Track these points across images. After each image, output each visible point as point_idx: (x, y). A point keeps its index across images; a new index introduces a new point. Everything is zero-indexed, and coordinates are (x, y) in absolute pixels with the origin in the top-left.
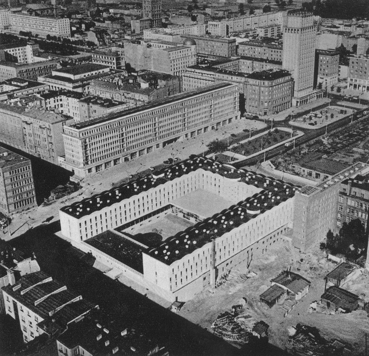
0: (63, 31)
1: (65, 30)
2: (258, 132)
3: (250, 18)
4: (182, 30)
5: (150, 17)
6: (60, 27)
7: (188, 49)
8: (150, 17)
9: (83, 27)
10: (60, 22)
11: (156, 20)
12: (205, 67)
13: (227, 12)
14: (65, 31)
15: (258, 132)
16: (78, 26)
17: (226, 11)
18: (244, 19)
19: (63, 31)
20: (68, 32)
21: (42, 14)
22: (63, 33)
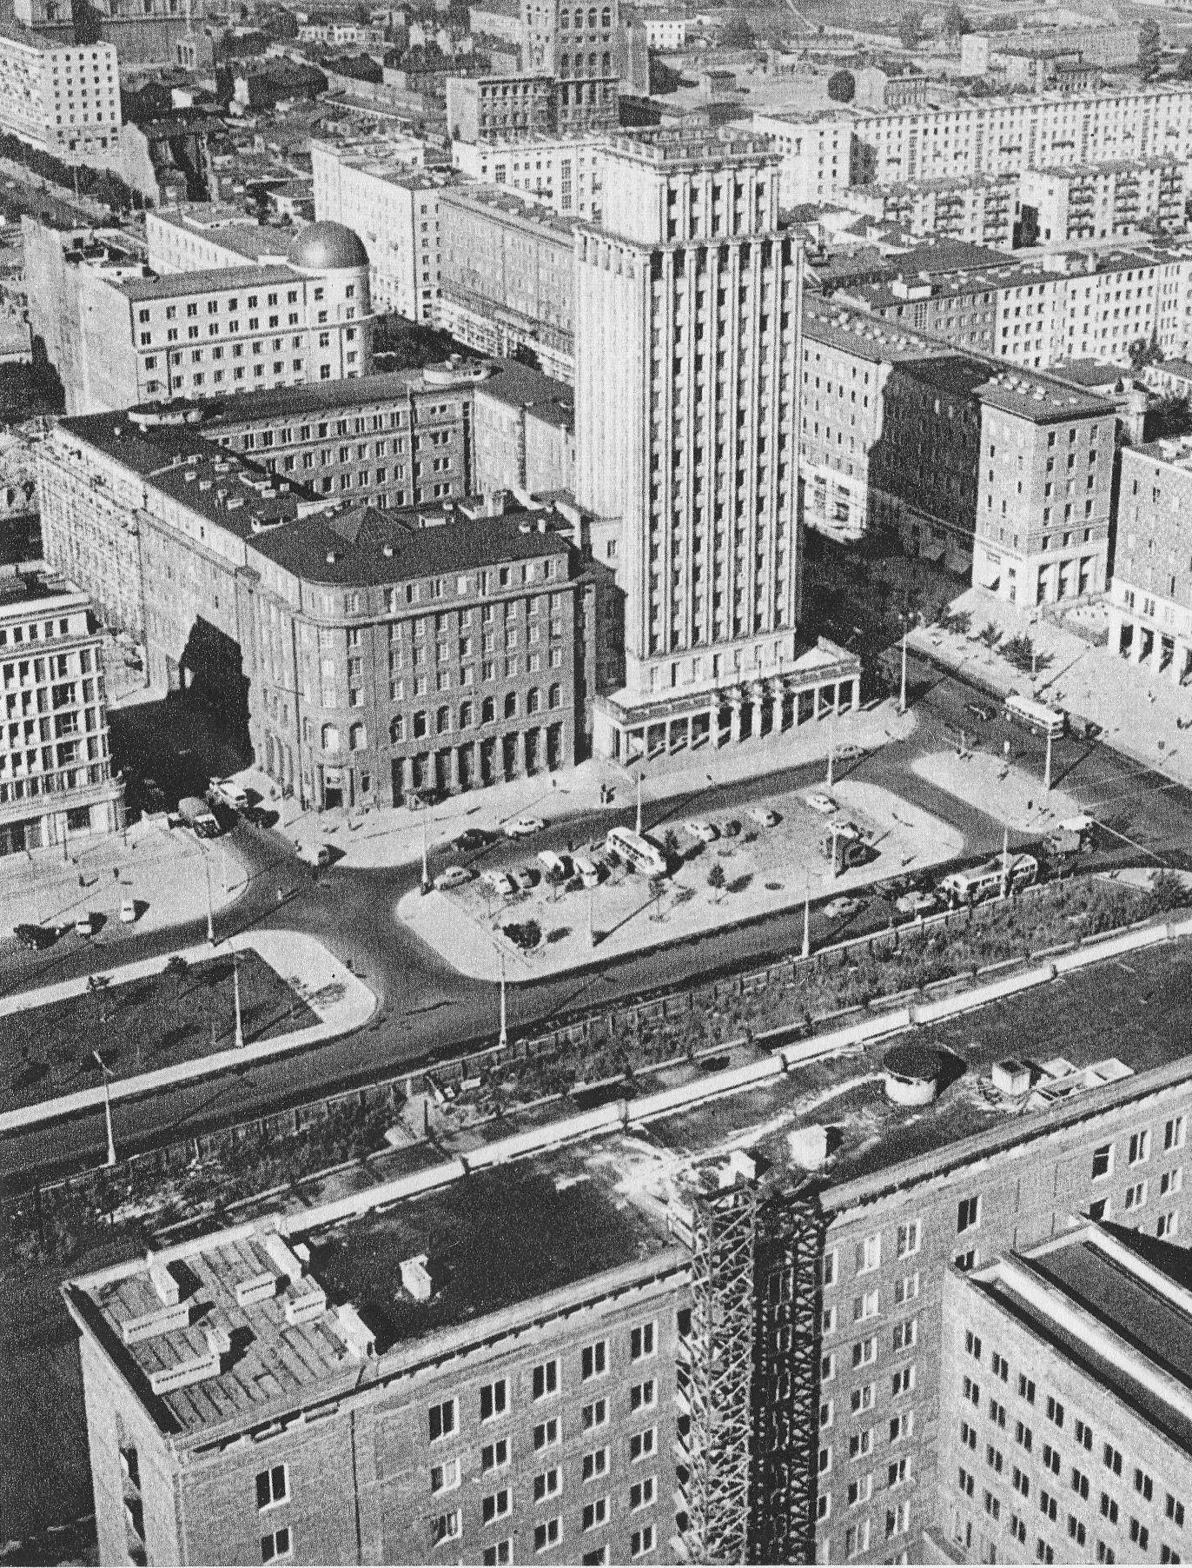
0: (79, 113)
1: (92, 106)
2: (669, 1068)
3: (1028, 114)
4: (557, 157)
5: (549, 68)
6: (63, 88)
7: (297, 287)
8: (549, 68)
9: (237, 95)
10: (61, 63)
11: (579, 85)
12: (151, 428)
13: (1050, 63)
14: (93, 111)
15: (669, 1068)
16: (210, 85)
17: (1047, 55)
18: (1087, 104)
19: (79, 113)
20: (106, 119)
21: (50, 16)
22: (79, 122)
